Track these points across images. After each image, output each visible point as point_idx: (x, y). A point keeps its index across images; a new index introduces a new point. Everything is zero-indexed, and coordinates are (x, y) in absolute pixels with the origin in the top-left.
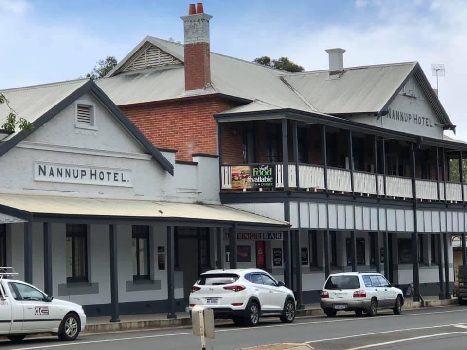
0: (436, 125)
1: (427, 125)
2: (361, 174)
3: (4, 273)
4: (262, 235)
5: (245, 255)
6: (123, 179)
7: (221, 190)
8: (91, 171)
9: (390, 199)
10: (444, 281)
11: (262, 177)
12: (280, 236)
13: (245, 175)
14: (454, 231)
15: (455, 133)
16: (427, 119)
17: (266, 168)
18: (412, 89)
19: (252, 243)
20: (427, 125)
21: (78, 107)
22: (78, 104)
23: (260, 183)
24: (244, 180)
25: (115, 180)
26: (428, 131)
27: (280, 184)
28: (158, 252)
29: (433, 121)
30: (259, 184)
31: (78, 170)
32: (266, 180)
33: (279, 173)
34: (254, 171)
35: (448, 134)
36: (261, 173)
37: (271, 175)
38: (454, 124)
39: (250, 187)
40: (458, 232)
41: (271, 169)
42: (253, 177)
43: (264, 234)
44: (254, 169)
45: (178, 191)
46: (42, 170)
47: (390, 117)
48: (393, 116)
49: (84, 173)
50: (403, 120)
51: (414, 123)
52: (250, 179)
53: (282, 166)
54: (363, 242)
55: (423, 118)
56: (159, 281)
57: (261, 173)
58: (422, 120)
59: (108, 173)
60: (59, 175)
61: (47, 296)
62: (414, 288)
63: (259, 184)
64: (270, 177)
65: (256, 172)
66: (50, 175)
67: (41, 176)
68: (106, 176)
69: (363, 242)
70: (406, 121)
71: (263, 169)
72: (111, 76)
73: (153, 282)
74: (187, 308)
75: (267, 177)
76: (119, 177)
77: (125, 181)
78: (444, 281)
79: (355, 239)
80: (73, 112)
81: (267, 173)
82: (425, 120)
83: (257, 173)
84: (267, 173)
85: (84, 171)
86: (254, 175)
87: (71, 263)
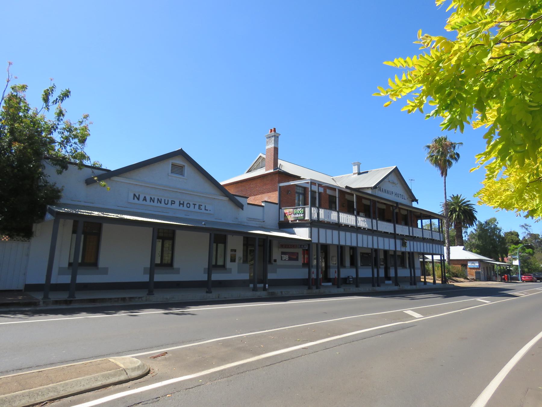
0: (407, 199)
1: (403, 198)
4: (297, 246)
5: (295, 257)
6: (206, 209)
8: (180, 202)
9: (381, 232)
10: (413, 275)
11: (299, 214)
12: (306, 247)
13: (290, 213)
14: (364, 246)
15: (418, 203)
16: (402, 195)
18: (393, 178)
19: (300, 251)
20: (403, 198)
21: (172, 165)
22: (172, 163)
23: (297, 217)
24: (290, 216)
25: (199, 209)
26: (404, 200)
27: (307, 218)
28: (231, 252)
29: (406, 196)
31: (168, 200)
33: (307, 212)
34: (295, 211)
35: (414, 204)
36: (298, 212)
37: (303, 213)
38: (417, 199)
39: (293, 220)
40: (430, 253)
41: (303, 210)
42: (294, 214)
43: (298, 245)
44: (295, 210)
45: (248, 219)
46: (136, 197)
47: (381, 191)
48: (383, 191)
49: (173, 202)
50: (388, 194)
52: (293, 215)
55: (400, 195)
56: (230, 269)
58: (399, 195)
59: (193, 204)
60: (152, 201)
64: (302, 214)
66: (143, 201)
67: (151, 203)
68: (192, 206)
70: (390, 194)
73: (226, 269)
75: (301, 214)
76: (203, 207)
77: (207, 210)
78: (413, 275)
79: (273, 260)
80: (167, 166)
81: (301, 212)
82: (401, 196)
84: (301, 212)
85: (174, 201)
86: (295, 213)
87: (160, 255)
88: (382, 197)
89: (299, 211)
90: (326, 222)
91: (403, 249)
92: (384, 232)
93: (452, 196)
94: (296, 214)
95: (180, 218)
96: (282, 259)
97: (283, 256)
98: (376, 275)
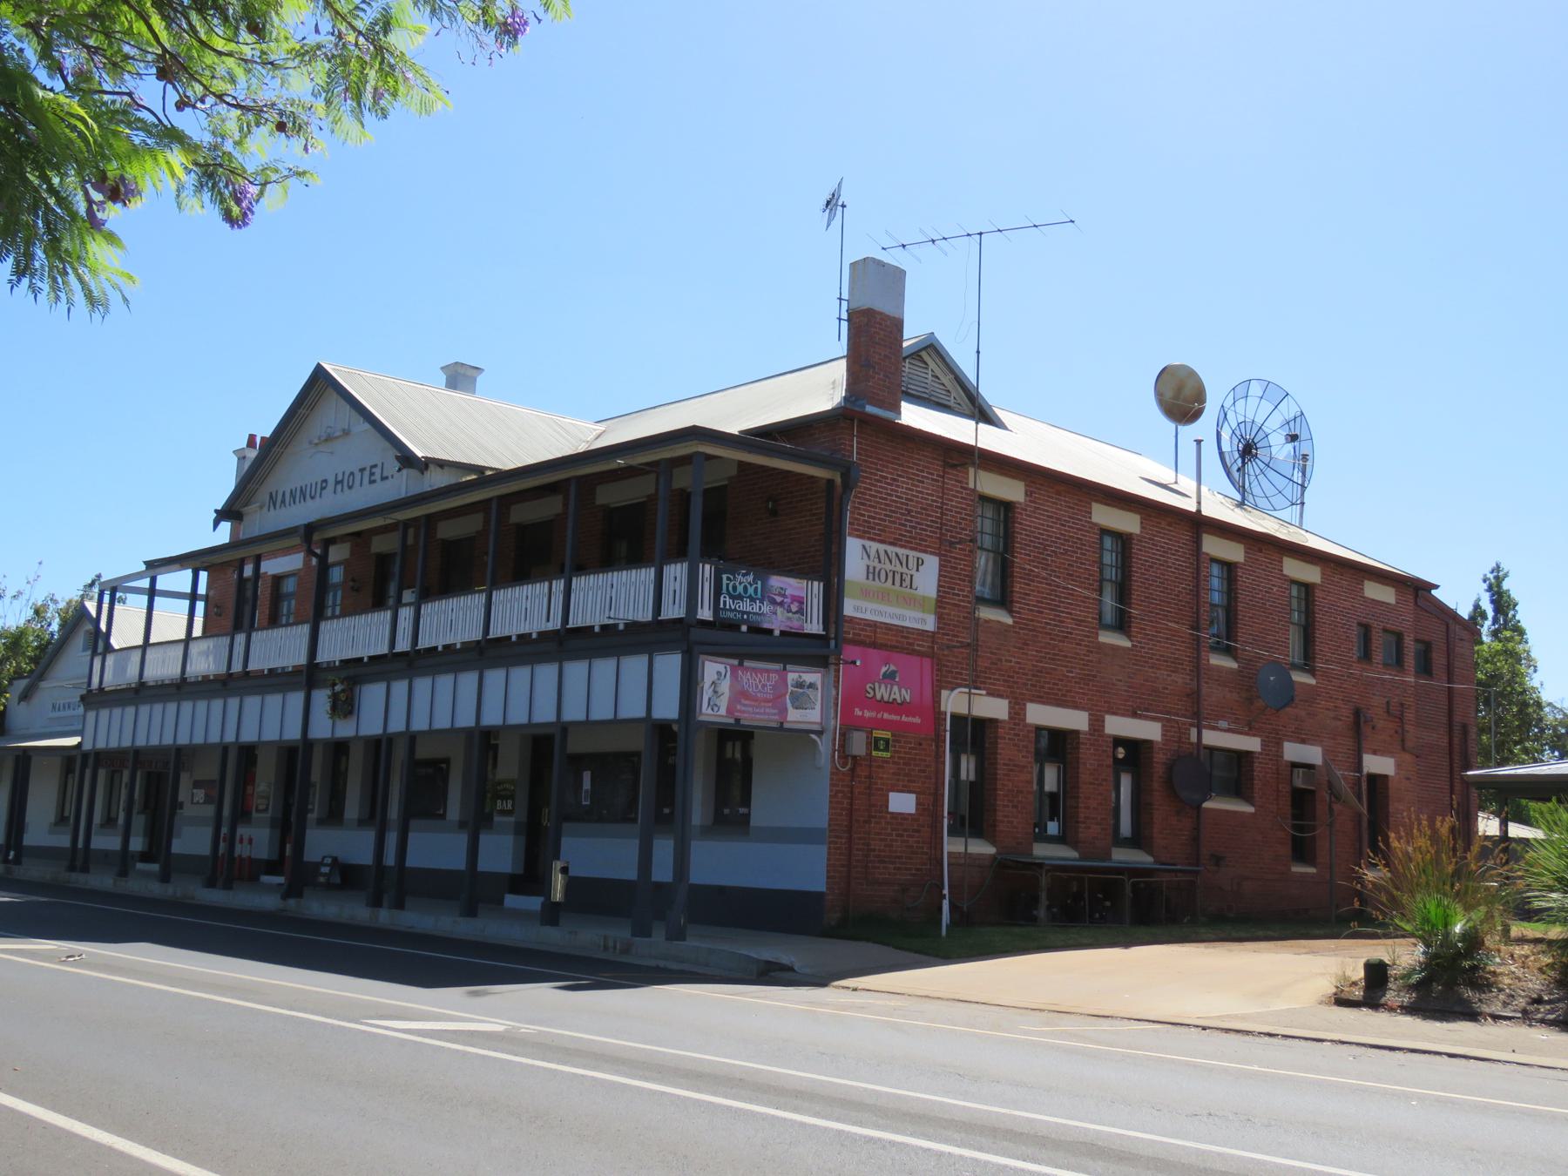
3: (1493, 700)
7: (204, 803)
10: (80, 844)
11: (753, 600)
23: (748, 613)
32: (760, 609)
34: (725, 581)
36: (740, 589)
38: (235, 459)
41: (759, 582)
54: (444, 766)
57: (740, 589)
62: (1378, 841)
65: (728, 585)
69: (444, 766)
71: (744, 580)
78: (80, 844)
83: (730, 589)
84: (751, 590)
88: (282, 527)
89: (745, 588)
90: (212, 677)
91: (345, 730)
92: (341, 661)
93: (828, 211)
94: (740, 597)
95: (58, 732)
96: (192, 803)
97: (195, 791)
98: (390, 859)
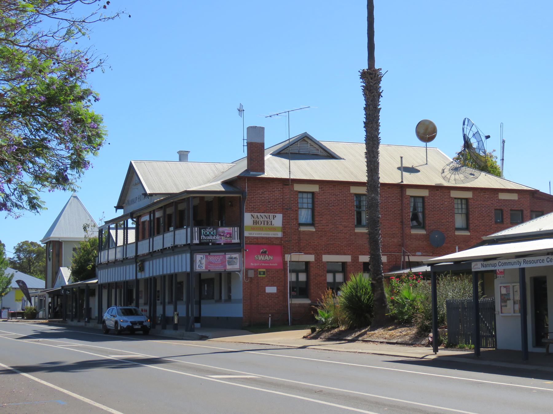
2: (178, 231)
11: (212, 235)
17: (212, 229)
23: (211, 240)
30: (210, 241)
32: (216, 238)
36: (208, 233)
41: (215, 230)
51: (42, 212)
53: (238, 228)
61: (270, 318)
63: (210, 241)
65: (204, 232)
69: (182, 284)
72: (330, 156)
74: (77, 258)
84: (212, 233)
94: (208, 235)
